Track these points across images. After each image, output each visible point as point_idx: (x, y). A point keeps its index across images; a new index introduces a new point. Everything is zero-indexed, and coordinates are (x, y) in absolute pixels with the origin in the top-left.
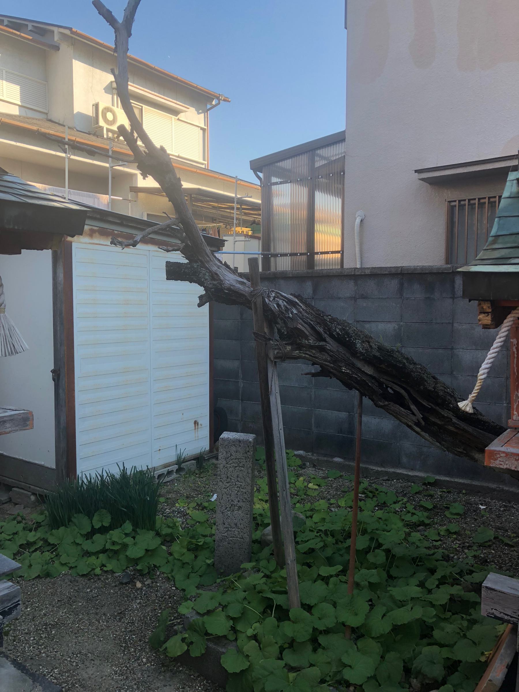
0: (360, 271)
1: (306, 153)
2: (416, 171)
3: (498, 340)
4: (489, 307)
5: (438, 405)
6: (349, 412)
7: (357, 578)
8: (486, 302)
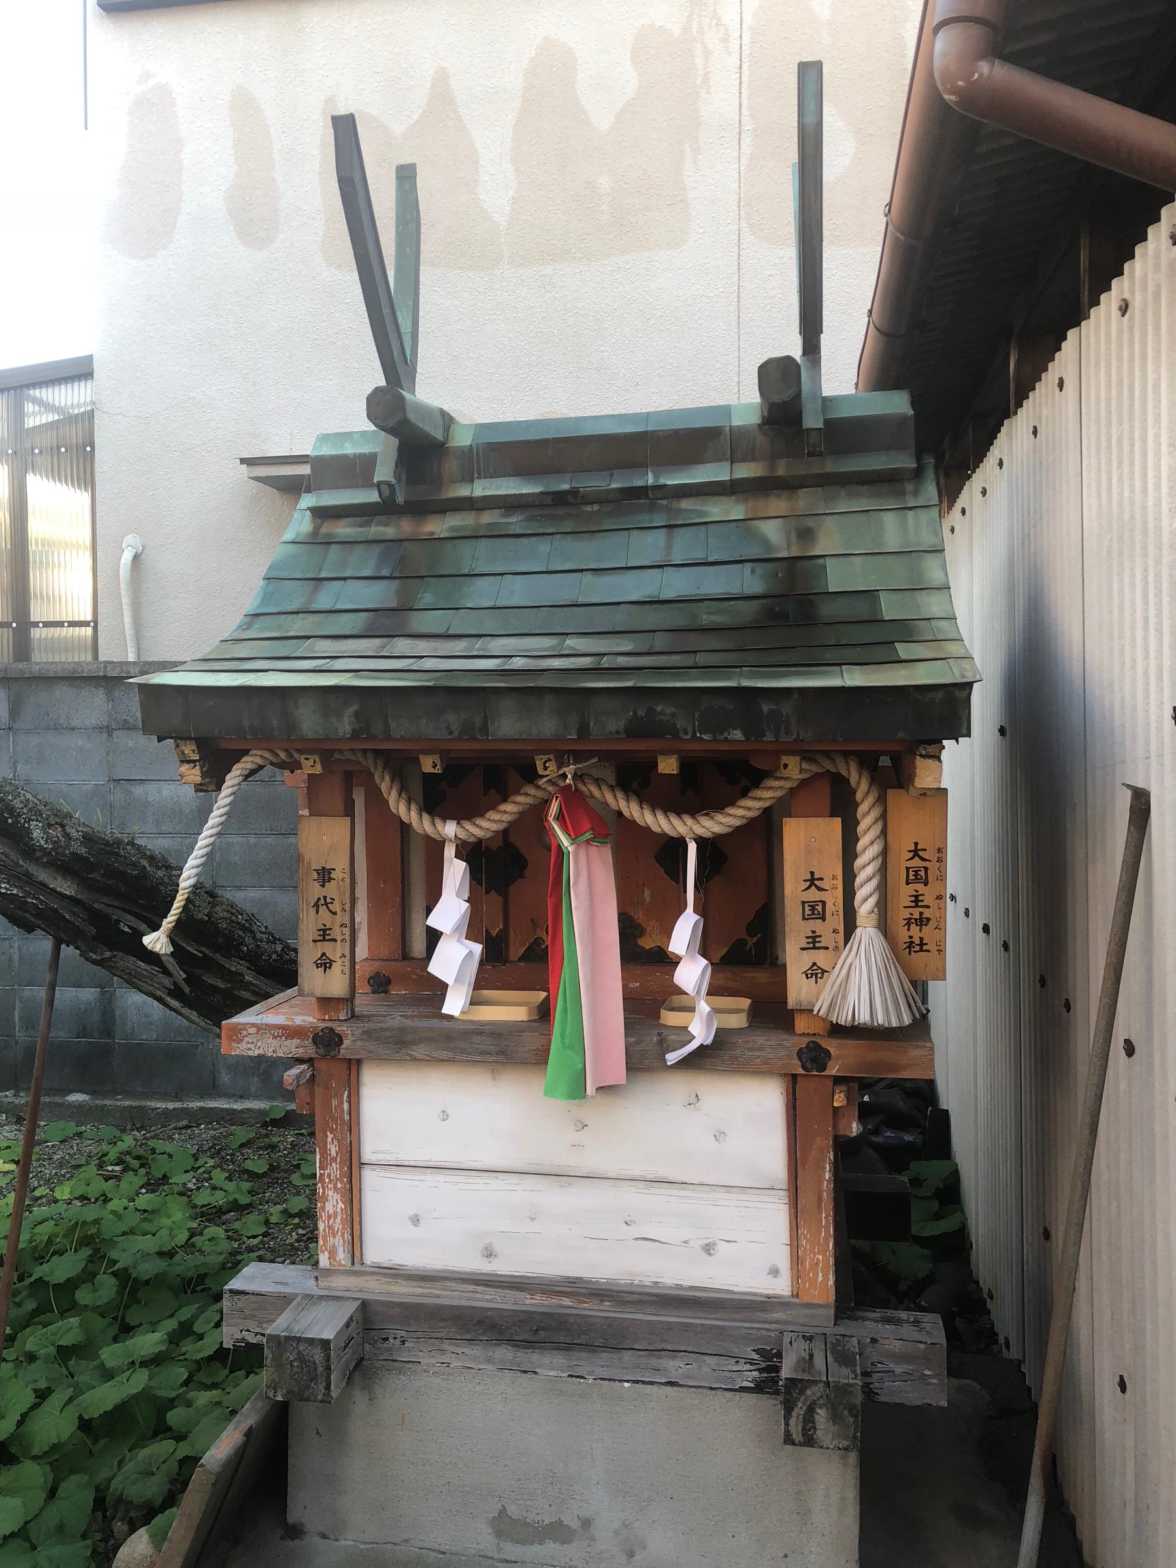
0: (118, 670)
1: (12, 392)
2: (243, 461)
3: (216, 813)
4: (193, 751)
5: (217, 948)
6: (102, 988)
7: (29, 1346)
8: (188, 742)
